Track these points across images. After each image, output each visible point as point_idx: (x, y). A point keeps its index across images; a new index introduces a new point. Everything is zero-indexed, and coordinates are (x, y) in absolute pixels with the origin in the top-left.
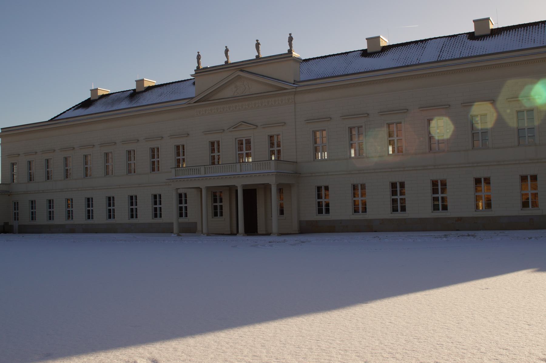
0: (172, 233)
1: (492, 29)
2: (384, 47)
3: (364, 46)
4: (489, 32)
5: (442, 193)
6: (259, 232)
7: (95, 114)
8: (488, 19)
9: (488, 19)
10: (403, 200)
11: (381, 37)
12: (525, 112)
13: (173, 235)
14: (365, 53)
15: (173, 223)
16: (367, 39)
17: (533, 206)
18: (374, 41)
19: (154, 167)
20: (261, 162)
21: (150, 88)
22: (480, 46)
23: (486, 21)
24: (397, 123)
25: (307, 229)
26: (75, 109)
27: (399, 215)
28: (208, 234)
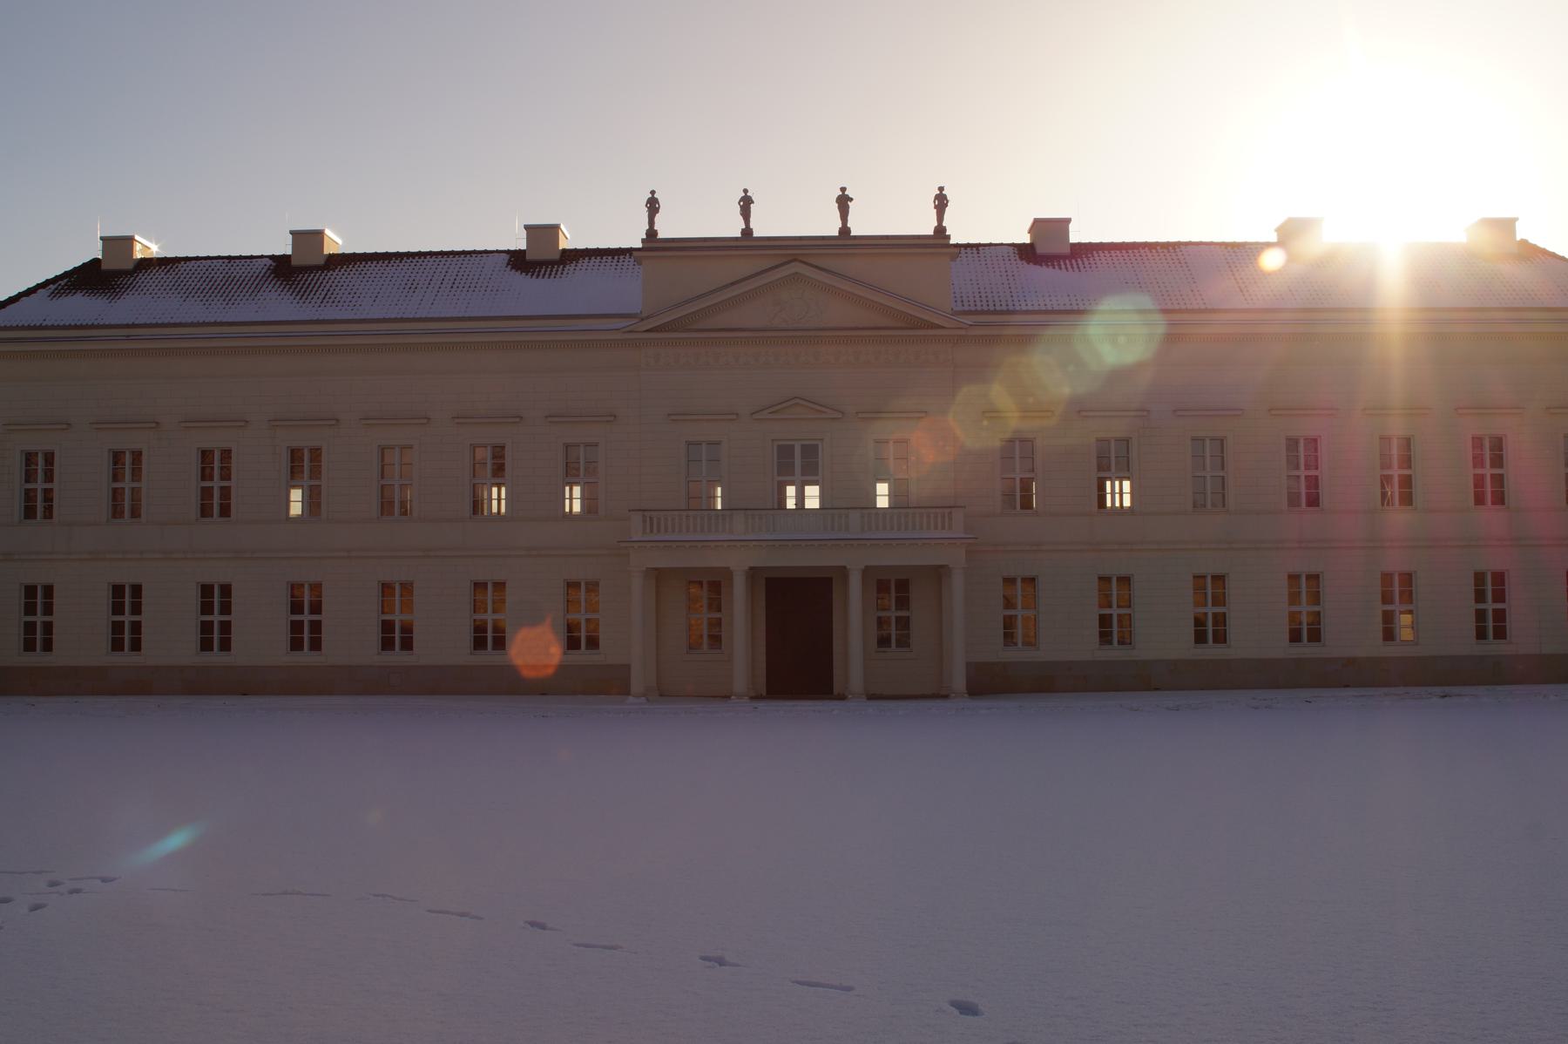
0: (628, 693)
1: (564, 251)
2: (331, 256)
3: (519, 242)
4: (1067, 251)
5: (494, 611)
6: (836, 691)
7: (192, 325)
8: (556, 228)
9: (556, 228)
10: (48, 627)
11: (328, 232)
12: (704, 446)
13: (631, 699)
14: (516, 260)
15: (627, 667)
16: (292, 232)
17: (1215, 641)
18: (308, 239)
19: (123, 506)
20: (654, 514)
21: (147, 264)
22: (532, 294)
23: (129, 241)
24: (403, 448)
25: (989, 683)
26: (53, 295)
27: (1211, 651)
28: (872, 697)
